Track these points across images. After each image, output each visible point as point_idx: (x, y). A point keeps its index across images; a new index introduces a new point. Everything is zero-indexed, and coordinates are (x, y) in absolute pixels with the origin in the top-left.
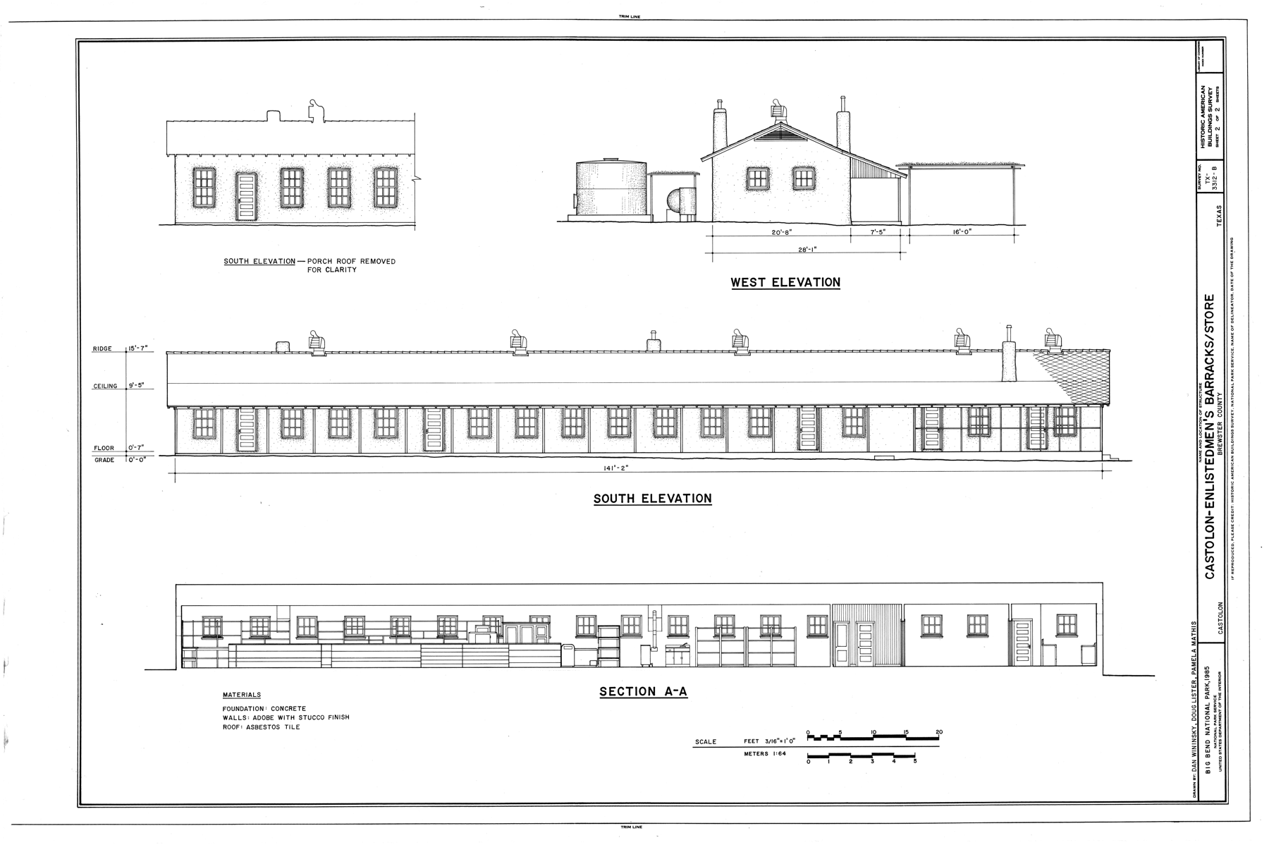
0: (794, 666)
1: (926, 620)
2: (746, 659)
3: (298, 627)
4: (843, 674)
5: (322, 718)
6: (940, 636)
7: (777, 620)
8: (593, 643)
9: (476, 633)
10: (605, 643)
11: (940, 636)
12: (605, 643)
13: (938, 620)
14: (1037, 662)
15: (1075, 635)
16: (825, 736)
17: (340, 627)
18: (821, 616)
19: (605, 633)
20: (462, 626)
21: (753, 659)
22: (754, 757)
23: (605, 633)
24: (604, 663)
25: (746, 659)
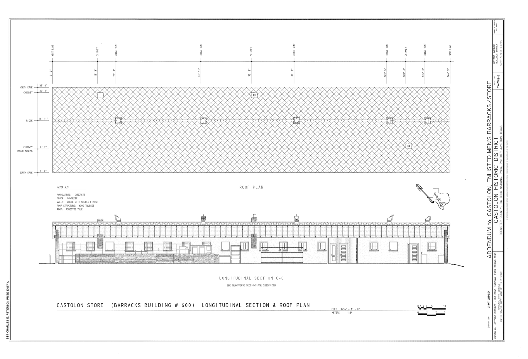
0: (302, 263)
1: (429, 244)
2: (282, 260)
3: (248, 246)
4: (334, 267)
5: (244, 285)
6: (377, 250)
7: (286, 244)
8: (229, 253)
9: (180, 250)
10: (233, 253)
11: (377, 250)
12: (233, 253)
13: (434, 244)
14: (420, 262)
15: (435, 250)
16: (428, 315)
17: (124, 246)
18: (323, 242)
19: (233, 248)
20: (174, 246)
21: (285, 260)
22: (497, 334)
23: (233, 248)
24: (233, 261)
25: (282, 260)
